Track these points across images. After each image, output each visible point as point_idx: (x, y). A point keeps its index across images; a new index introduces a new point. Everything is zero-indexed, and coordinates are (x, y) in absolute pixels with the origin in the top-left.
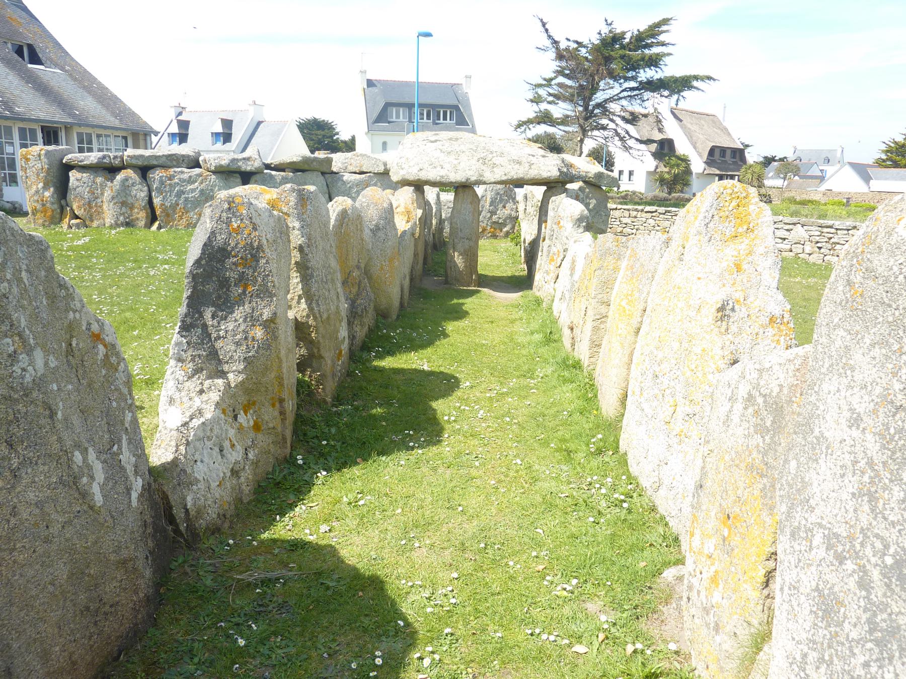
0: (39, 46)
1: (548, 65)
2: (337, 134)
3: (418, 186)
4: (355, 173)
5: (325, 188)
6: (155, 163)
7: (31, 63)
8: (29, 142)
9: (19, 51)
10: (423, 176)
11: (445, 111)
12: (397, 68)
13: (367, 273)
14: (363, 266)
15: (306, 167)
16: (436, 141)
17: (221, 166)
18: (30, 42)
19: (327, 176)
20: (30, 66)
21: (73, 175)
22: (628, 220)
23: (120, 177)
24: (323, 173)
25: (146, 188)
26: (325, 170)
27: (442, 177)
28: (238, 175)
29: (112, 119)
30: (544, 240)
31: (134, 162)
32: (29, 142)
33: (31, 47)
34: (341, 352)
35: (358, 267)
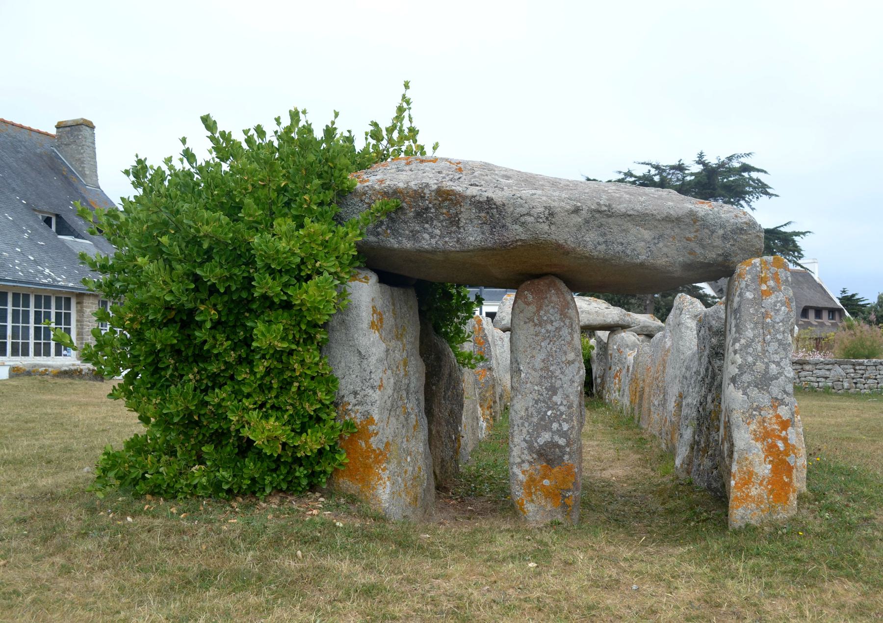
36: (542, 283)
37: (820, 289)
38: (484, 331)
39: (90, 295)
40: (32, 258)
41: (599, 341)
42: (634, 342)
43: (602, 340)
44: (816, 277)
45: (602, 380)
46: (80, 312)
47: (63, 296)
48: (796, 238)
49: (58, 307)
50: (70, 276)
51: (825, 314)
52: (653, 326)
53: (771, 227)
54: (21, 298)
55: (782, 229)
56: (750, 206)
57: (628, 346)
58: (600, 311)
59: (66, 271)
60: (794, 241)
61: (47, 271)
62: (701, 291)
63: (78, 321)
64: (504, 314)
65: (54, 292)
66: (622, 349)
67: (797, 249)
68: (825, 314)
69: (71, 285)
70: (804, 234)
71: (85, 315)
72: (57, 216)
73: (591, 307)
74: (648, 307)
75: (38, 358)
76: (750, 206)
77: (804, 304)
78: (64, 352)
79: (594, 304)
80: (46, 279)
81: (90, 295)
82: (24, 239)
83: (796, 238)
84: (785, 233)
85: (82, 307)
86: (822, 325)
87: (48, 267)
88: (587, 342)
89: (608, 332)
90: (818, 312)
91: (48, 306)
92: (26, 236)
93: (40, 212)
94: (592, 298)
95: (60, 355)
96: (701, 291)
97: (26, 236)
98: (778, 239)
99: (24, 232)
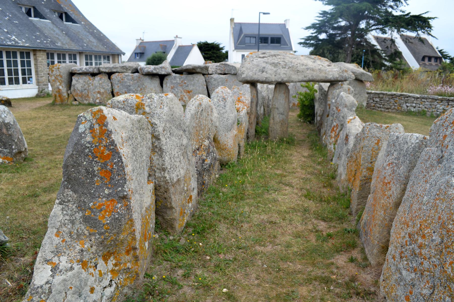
0: (70, 13)
1: (235, 51)
2: (222, 49)
3: (253, 84)
4: (221, 74)
5: (205, 83)
6: (115, 70)
7: (66, 21)
8: (62, 60)
9: (61, 17)
10: (256, 77)
11: (273, 39)
12: (249, 17)
13: (215, 140)
14: (212, 137)
15: (194, 71)
16: (263, 57)
17: (149, 72)
18: (66, 11)
19: (206, 76)
20: (65, 23)
21: (74, 79)
22: (378, 100)
23: (97, 78)
24: (204, 75)
25: (110, 85)
26: (204, 72)
27: (266, 78)
28: (158, 77)
29: (102, 47)
30: (328, 116)
31: (104, 70)
32: (62, 60)
33: (66, 13)
34: (191, 197)
35: (208, 138)
36: (80, 72)
37: (431, 47)
38: (109, 136)
39: (40, 50)
40: (6, 30)
41: (321, 89)
42: (353, 102)
43: (323, 89)
44: (430, 42)
45: (321, 118)
46: (36, 60)
47: (25, 51)
48: (430, 21)
49: (22, 57)
50: (28, 39)
51: (433, 60)
52: (358, 72)
53: (417, 14)
54: (11, 53)
55: (423, 16)
56: (406, 3)
57: (346, 106)
58: (323, 68)
59: (27, 37)
60: (428, 22)
61: (14, 37)
62: (375, 47)
63: (35, 65)
64: (244, 69)
65: (18, 49)
66: (340, 108)
67: (430, 27)
68: (433, 60)
69: (27, 45)
70: (434, 18)
71: (38, 61)
72: (34, 8)
73: (315, 64)
74: (348, 55)
75: (11, 86)
76: (406, 3)
77: (424, 54)
78: (28, 82)
79: (318, 62)
80: (10, 42)
81: (40, 50)
82: (5, 20)
83: (430, 21)
84: (425, 18)
85: (36, 57)
86: (431, 65)
87: (15, 35)
88: (313, 86)
89: (328, 84)
90: (430, 58)
91: (15, 56)
92: (7, 18)
93: (24, 5)
94: (317, 57)
95: (26, 83)
96: (375, 47)
97: (7, 18)
98: (421, 21)
99: (6, 16)
